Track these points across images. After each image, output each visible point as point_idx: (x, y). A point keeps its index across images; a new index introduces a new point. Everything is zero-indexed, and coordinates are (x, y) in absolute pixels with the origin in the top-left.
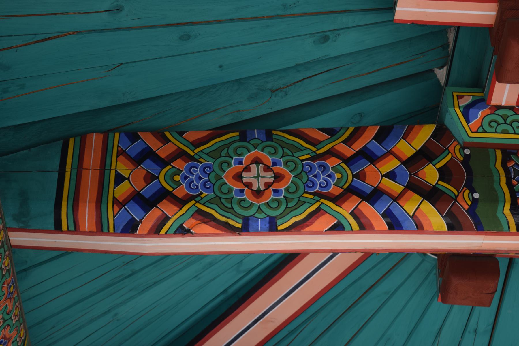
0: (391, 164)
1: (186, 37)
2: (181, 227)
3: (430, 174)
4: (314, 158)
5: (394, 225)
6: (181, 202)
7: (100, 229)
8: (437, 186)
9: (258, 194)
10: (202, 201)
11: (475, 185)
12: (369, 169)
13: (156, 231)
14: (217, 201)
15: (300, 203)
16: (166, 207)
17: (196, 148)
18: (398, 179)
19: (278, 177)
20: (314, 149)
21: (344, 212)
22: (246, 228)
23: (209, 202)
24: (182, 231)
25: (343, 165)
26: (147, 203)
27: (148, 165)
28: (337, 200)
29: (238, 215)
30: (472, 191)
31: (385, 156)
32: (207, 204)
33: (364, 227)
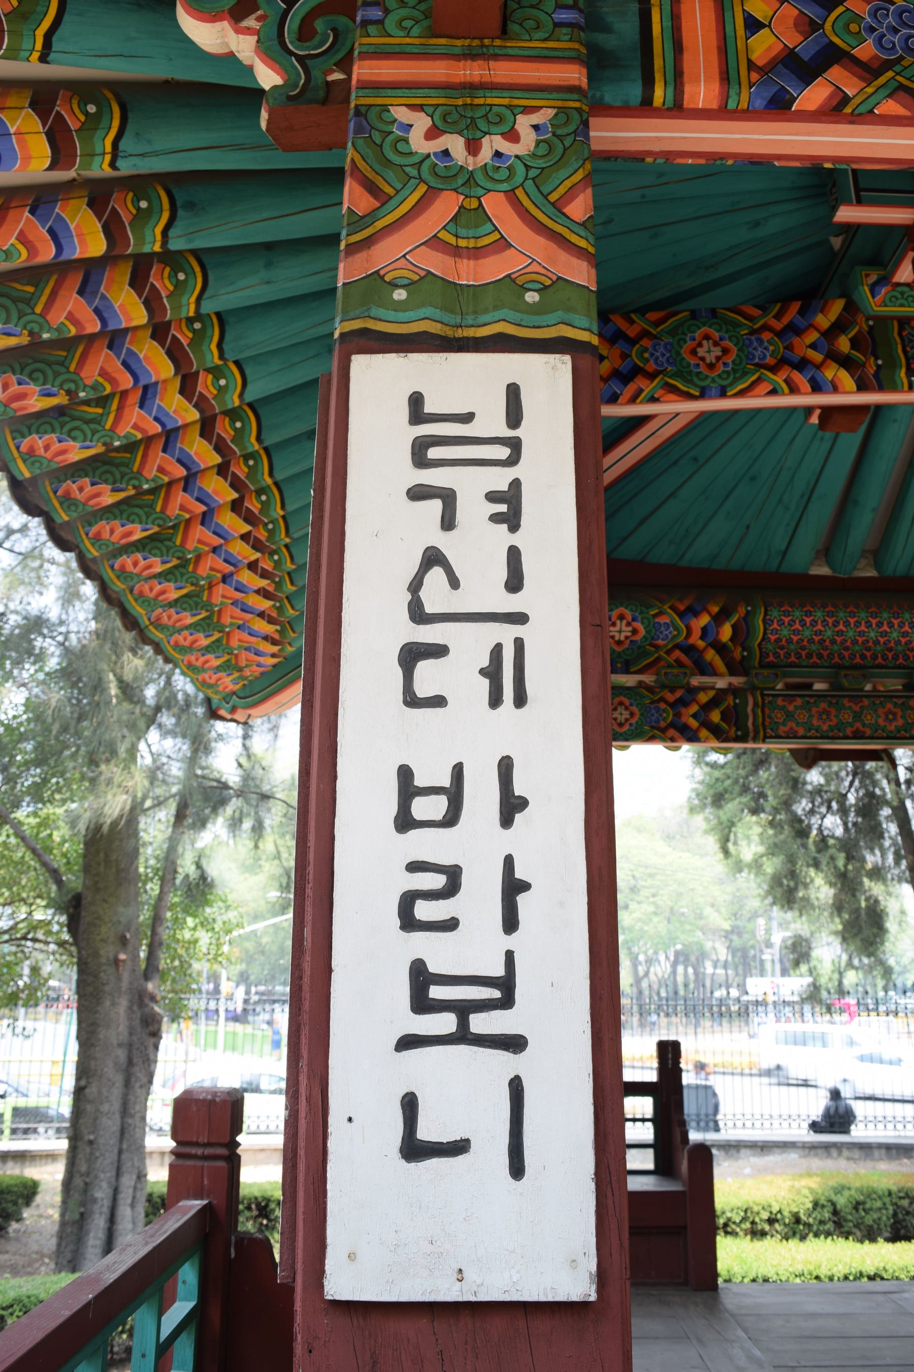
3: (844, 344)
5: (816, 388)
6: (652, 376)
9: (711, 366)
12: (796, 340)
13: (633, 400)
14: (677, 375)
15: (745, 374)
16: (640, 382)
19: (726, 351)
21: (779, 379)
22: (703, 395)
24: (653, 400)
27: (620, 346)
28: (774, 369)
29: (696, 385)
33: (794, 390)
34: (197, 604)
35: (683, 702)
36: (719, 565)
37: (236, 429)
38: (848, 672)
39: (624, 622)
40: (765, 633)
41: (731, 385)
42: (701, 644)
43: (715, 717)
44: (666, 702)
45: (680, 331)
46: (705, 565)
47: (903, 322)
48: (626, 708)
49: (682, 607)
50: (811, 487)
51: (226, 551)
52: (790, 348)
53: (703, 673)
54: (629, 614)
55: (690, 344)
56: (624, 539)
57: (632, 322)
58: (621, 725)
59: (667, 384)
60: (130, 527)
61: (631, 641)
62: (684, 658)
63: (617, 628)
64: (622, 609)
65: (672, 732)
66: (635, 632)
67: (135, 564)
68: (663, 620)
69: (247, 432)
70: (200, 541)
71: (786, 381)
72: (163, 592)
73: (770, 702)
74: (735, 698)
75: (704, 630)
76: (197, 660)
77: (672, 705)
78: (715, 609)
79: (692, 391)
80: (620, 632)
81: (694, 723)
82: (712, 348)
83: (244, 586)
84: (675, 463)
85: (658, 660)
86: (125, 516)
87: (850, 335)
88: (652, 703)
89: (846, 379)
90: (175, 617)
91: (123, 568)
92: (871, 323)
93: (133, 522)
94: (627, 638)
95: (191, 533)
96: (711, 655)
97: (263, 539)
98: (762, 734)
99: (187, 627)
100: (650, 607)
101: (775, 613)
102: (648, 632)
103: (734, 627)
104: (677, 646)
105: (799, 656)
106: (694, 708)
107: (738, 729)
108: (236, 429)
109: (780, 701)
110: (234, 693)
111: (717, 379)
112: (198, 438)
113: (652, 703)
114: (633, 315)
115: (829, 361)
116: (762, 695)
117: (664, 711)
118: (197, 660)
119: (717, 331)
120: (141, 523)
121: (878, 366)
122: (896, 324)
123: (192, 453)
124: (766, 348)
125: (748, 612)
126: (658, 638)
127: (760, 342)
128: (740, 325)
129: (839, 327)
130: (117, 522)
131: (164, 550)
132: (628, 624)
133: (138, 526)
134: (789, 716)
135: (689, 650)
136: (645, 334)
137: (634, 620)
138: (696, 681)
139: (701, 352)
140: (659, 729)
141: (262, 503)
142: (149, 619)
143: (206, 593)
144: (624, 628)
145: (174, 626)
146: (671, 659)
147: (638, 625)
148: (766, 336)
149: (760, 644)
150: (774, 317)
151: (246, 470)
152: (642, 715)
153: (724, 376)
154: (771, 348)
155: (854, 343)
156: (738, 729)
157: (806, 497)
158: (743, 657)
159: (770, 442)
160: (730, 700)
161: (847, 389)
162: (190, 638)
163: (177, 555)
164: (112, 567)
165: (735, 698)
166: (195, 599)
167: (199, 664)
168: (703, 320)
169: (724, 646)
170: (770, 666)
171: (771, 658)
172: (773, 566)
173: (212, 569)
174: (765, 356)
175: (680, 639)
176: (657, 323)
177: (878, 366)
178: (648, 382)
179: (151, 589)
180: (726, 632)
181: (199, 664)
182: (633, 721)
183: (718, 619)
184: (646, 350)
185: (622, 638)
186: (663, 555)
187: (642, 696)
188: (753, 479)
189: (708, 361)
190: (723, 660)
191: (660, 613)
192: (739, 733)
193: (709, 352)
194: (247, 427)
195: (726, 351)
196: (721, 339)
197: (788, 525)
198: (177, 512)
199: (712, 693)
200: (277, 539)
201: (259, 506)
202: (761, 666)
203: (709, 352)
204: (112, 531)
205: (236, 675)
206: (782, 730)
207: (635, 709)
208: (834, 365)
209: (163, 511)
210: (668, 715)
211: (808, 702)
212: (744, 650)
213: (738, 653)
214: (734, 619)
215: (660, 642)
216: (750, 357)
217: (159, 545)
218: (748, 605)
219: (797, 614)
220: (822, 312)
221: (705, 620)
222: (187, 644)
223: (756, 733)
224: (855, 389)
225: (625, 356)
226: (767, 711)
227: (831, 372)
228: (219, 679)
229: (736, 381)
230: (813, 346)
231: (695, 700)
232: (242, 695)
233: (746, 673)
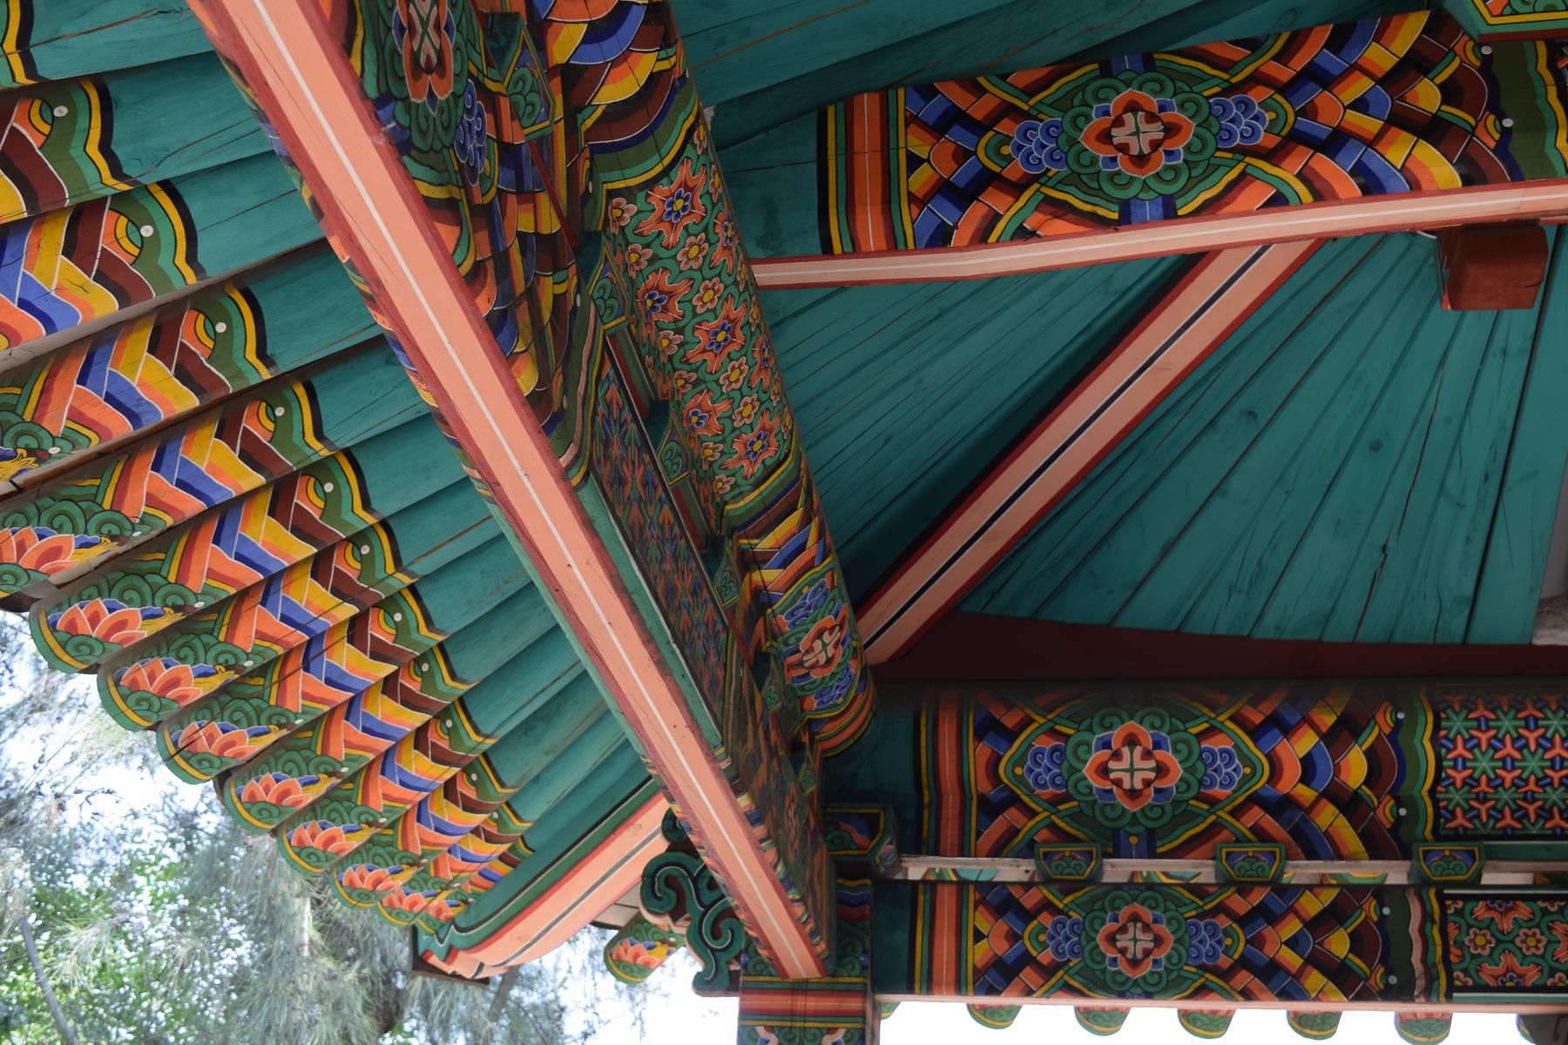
0: (1359, 86)
2: (1021, 228)
3: (1427, 96)
5: (1372, 187)
7: (893, 245)
9: (1141, 160)
12: (1322, 98)
13: (981, 238)
14: (1072, 180)
15: (1211, 169)
16: (993, 200)
19: (1171, 130)
21: (1286, 174)
22: (1126, 219)
23: (1062, 183)
24: (1023, 235)
26: (962, 196)
27: (957, 136)
29: (1111, 199)
33: (1322, 195)
34: (259, 712)
35: (1266, 914)
36: (1339, 633)
37: (216, 337)
39: (1138, 750)
40: (1439, 768)
41: (1183, 192)
42: (1306, 794)
43: (1339, 944)
44: (1231, 914)
45: (1077, 101)
46: (1312, 635)
47: (1558, 42)
48: (1146, 928)
49: (1257, 718)
50: (1502, 457)
51: (285, 600)
52: (1309, 112)
53: (1312, 854)
54: (1147, 736)
55: (1097, 122)
56: (1138, 587)
57: (980, 91)
58: (1135, 963)
59: (1048, 200)
60: (54, 538)
61: (1158, 791)
62: (1270, 823)
63: (1125, 764)
64: (1133, 725)
65: (1244, 978)
66: (1161, 770)
67: (94, 620)
68: (1217, 744)
69: (238, 341)
70: (212, 574)
71: (1300, 176)
72: (174, 683)
73: (1459, 913)
74: (1381, 905)
75: (1308, 762)
76: (313, 836)
77: (1244, 921)
78: (1329, 720)
79: (1101, 212)
80: (1131, 770)
81: (1292, 959)
82: (1144, 127)
83: (343, 674)
84: (1212, 424)
85: (1216, 827)
86: (45, 517)
87: (1440, 79)
88: (1200, 916)
89: (1436, 165)
90: (221, 738)
91: (72, 628)
92: (1486, 50)
93: (60, 529)
94: (1147, 783)
95: (195, 556)
96: (1328, 817)
97: (353, 575)
98: (1443, 981)
99: (313, 809)
100: (1189, 717)
101: (1457, 724)
102: (1190, 770)
103: (1370, 754)
104: (1255, 800)
105: (1520, 814)
106: (1292, 927)
107: (1389, 972)
108: (216, 337)
109: (1480, 908)
110: (452, 921)
111: (1153, 183)
112: (146, 354)
113: (1200, 916)
114: (981, 80)
115: (1394, 129)
116: (1441, 898)
117: (1226, 933)
118: (313, 836)
119: (1155, 93)
120: (75, 531)
121: (1505, 132)
122: (1542, 48)
123: (134, 385)
124: (1256, 118)
125: (1398, 723)
126: (1212, 784)
127: (1247, 106)
128: (1201, 79)
129: (1415, 65)
130: (32, 530)
131: (146, 589)
132: (1147, 755)
133: (71, 539)
134: (1503, 941)
135: (1281, 806)
136: (1007, 111)
138: (1300, 871)
139: (1119, 135)
140: (1216, 971)
141: (326, 497)
142: (175, 744)
143: (275, 688)
144: (1138, 764)
145: (220, 756)
146: (1242, 826)
147: (1168, 756)
148: (1257, 95)
149: (1432, 791)
150: (1275, 58)
151: (271, 426)
152: (1179, 941)
153: (1170, 176)
154: (1269, 116)
155: (1450, 92)
156: (1389, 972)
157: (1495, 480)
158: (1399, 818)
159: (1396, 366)
160: (1370, 910)
161: (1441, 185)
162: (276, 788)
163: (169, 601)
164: (53, 626)
165: (1381, 905)
166: (255, 702)
167: (317, 844)
168: (1123, 76)
169: (1356, 795)
170: (1458, 836)
171: (1460, 820)
172: (1453, 630)
173: (261, 635)
174: (1255, 131)
175: (1260, 784)
176: (1031, 91)
177: (1505, 132)
178: (1010, 199)
179: (152, 677)
180: (1355, 768)
181: (317, 844)
182: (1161, 956)
183: (1338, 739)
184: (1007, 140)
185: (1138, 785)
186: (1220, 616)
187: (1180, 903)
188: (1375, 447)
189: (1134, 151)
190: (1355, 826)
191: (1211, 731)
192: (1393, 980)
193: (1137, 134)
194: (238, 331)
195: (1171, 130)
196: (1162, 108)
197: (1468, 540)
198: (144, 509)
199: (1329, 896)
200: (380, 575)
201: (321, 504)
202: (1438, 836)
203: (1137, 133)
204: (21, 548)
205: (409, 873)
206: (1488, 973)
207: (1164, 929)
208: (1407, 139)
209: (116, 507)
210: (1236, 941)
211: (1545, 912)
212: (1399, 803)
213: (1386, 812)
214: (1369, 739)
215: (1217, 791)
216: (1225, 135)
217: (139, 582)
218: (1397, 710)
219: (1507, 724)
220: (1377, 39)
221: (1306, 742)
222: (270, 798)
223: (1431, 979)
224: (1460, 183)
225: (962, 155)
226: (1451, 929)
227: (1399, 149)
228: (378, 882)
229: (1192, 184)
230: (1360, 105)
231: (1292, 910)
232: (463, 925)
233: (1405, 853)
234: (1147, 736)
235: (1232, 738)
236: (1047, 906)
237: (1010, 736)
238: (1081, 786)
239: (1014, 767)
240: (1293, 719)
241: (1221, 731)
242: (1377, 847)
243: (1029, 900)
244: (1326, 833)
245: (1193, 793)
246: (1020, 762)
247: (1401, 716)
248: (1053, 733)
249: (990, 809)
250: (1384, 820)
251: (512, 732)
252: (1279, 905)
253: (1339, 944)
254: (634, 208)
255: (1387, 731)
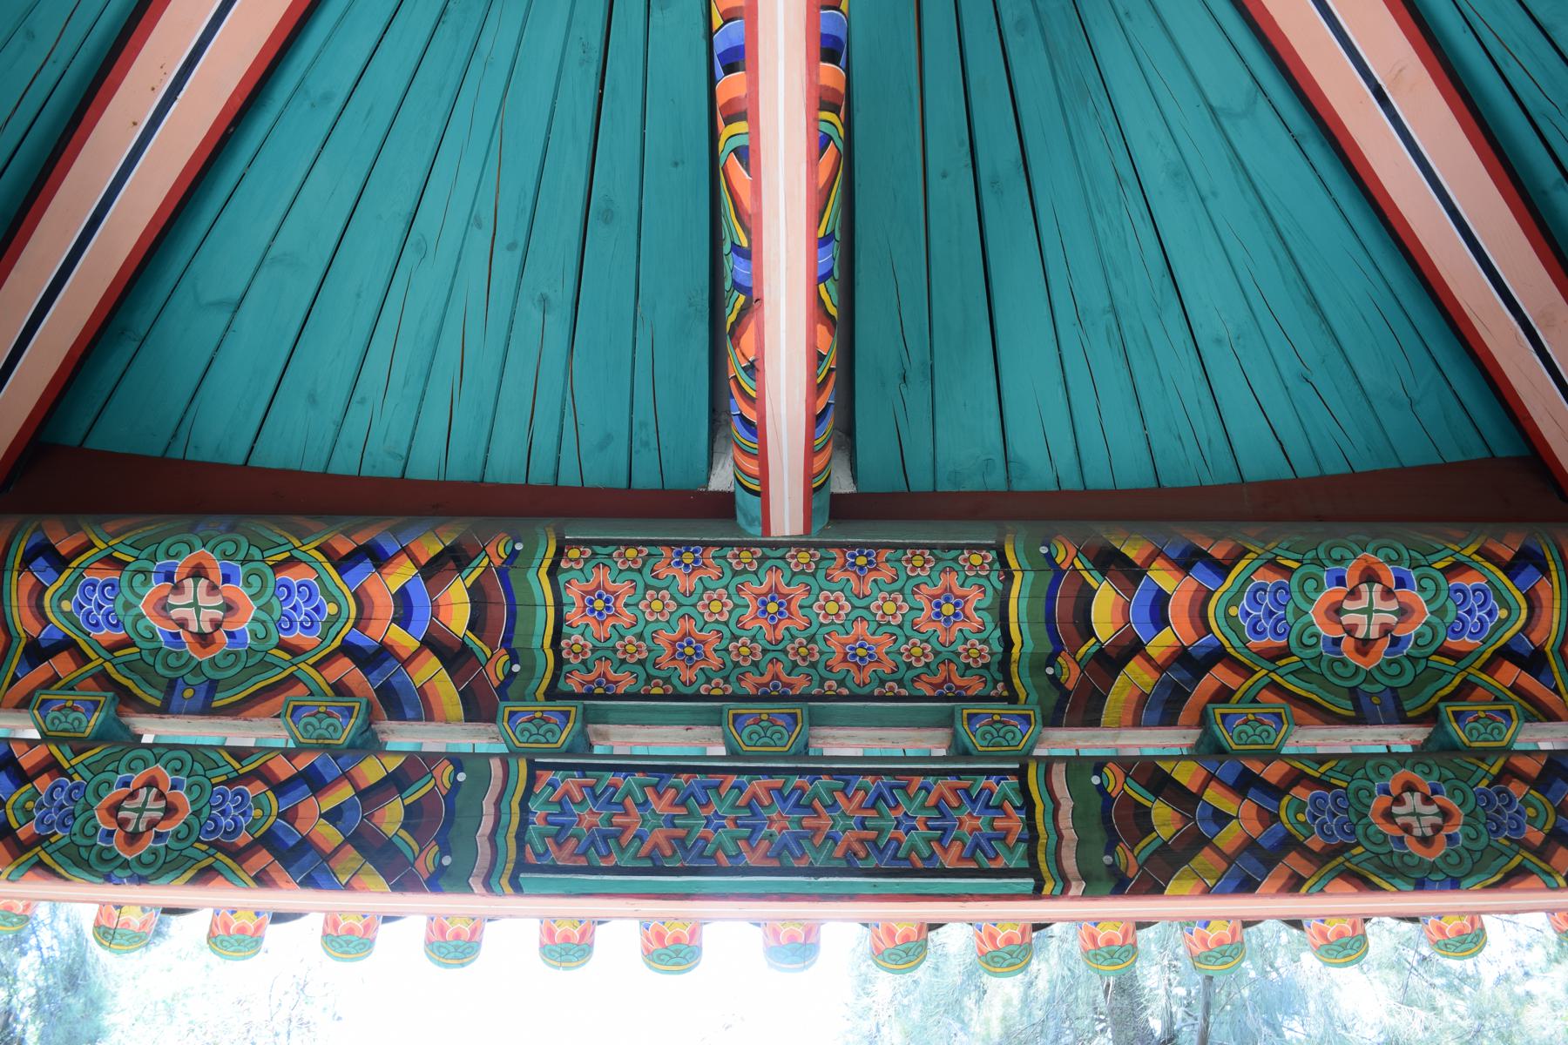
1: (608, 216)
3: (391, 817)
4: (229, 782)
8: (395, 840)
10: (50, 850)
11: (1098, 801)
17: (76, 756)
18: (1210, 811)
20: (237, 766)
25: (270, 794)
30: (1101, 788)
31: (337, 781)
32: (57, 855)
38: (974, 708)
42: (404, 640)
49: (1507, 554)
65: (263, 858)
80: (1368, 611)
81: (329, 835)
85: (292, 680)
96: (429, 670)
103: (476, 592)
125: (514, 554)
135: (373, 658)
137: (1401, 583)
180: (455, 607)
183: (434, 571)
191: (291, 562)
202: (552, 694)
221: (401, 574)
234: (1389, 574)
235: (315, 572)
236: (51, 766)
237: (1222, 569)
238: (141, 626)
239: (60, 599)
240: (391, 547)
241: (1471, 568)
242: (478, 707)
243: (27, 760)
244: (421, 690)
245: (274, 641)
246: (1234, 601)
247: (519, 547)
248: (1273, 564)
249: (37, 653)
250: (492, 677)
251: (1235, 564)
252: (332, 770)
253: (391, 817)
254: (576, 636)
255: (498, 562)
